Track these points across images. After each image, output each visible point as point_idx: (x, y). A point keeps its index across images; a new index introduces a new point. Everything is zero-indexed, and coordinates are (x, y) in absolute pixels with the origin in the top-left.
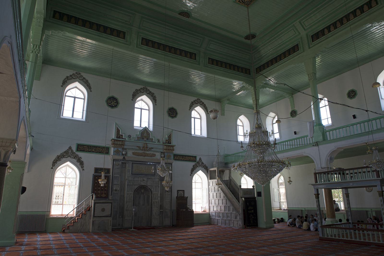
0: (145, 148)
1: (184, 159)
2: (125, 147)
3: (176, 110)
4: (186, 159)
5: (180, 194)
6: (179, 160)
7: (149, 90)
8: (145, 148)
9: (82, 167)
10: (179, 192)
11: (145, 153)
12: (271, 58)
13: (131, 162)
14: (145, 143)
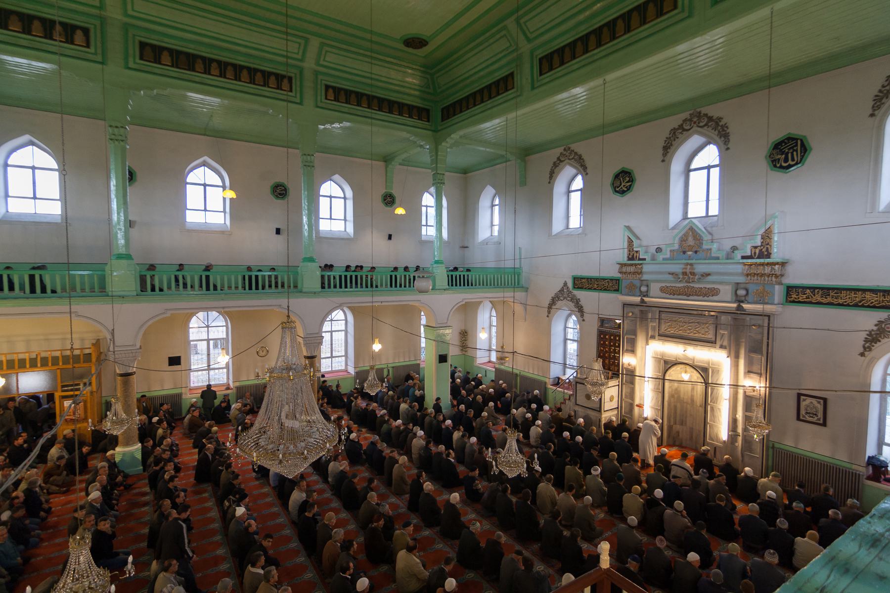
0: (688, 275)
1: (829, 299)
2: (645, 277)
3: (801, 140)
4: (841, 301)
5: (807, 406)
6: (811, 303)
7: (706, 115)
8: (688, 275)
9: (582, 316)
10: (819, 403)
11: (688, 288)
12: (476, 87)
13: (658, 310)
14: (687, 264)
